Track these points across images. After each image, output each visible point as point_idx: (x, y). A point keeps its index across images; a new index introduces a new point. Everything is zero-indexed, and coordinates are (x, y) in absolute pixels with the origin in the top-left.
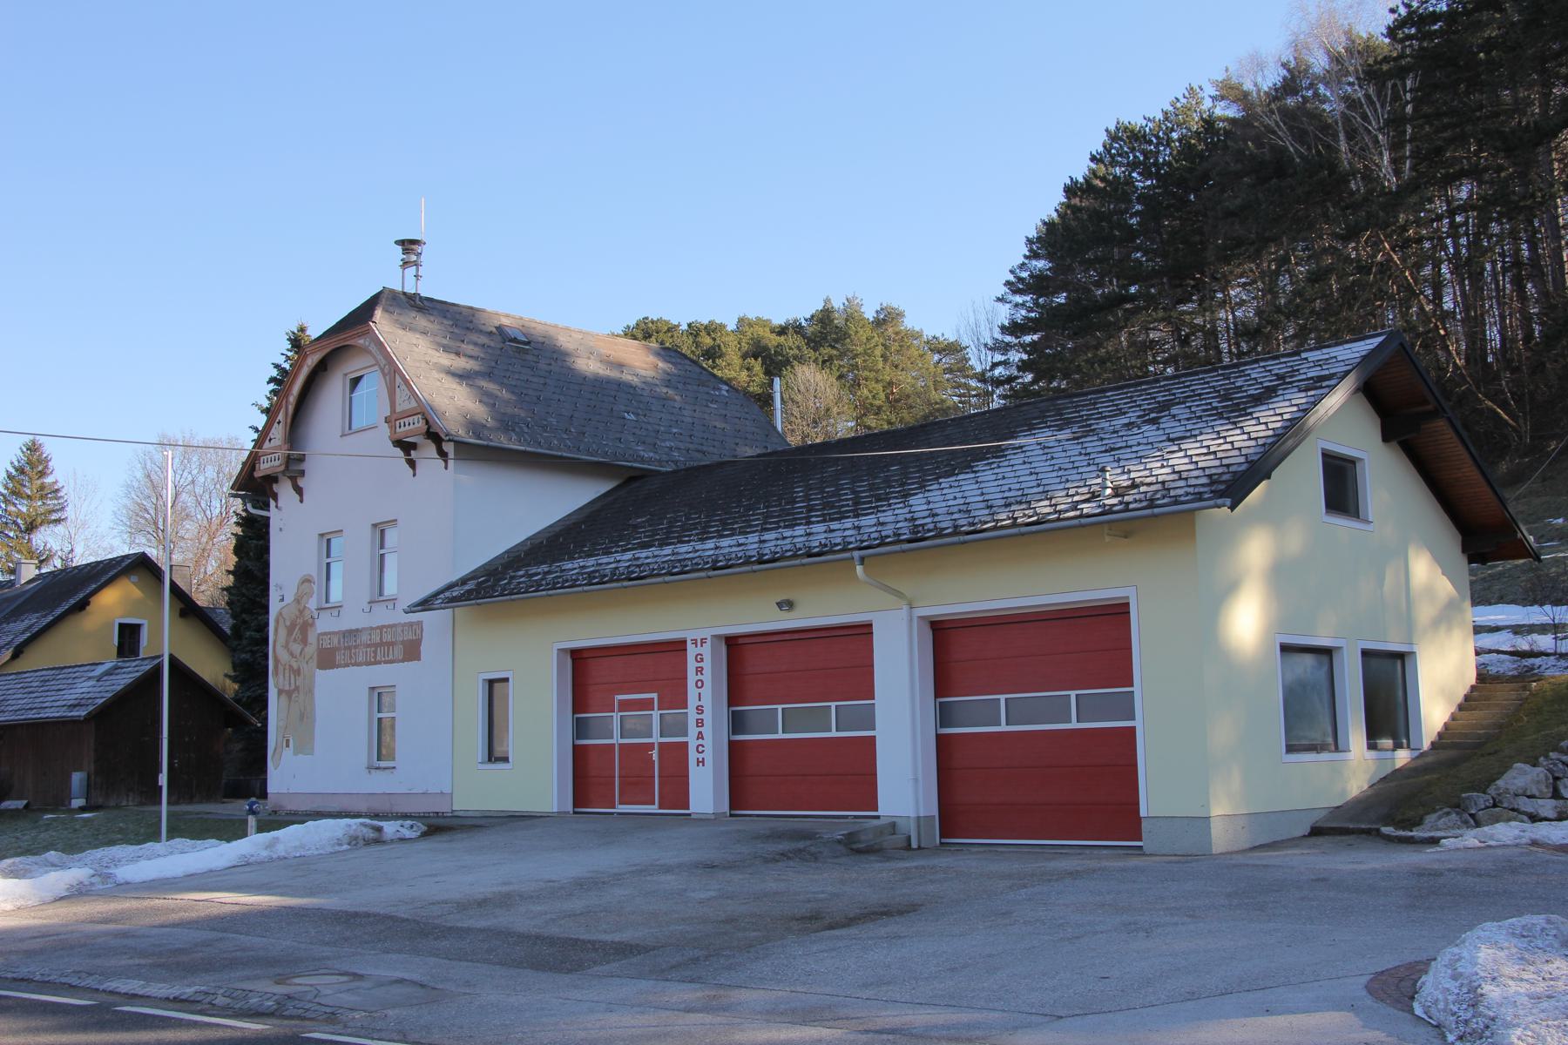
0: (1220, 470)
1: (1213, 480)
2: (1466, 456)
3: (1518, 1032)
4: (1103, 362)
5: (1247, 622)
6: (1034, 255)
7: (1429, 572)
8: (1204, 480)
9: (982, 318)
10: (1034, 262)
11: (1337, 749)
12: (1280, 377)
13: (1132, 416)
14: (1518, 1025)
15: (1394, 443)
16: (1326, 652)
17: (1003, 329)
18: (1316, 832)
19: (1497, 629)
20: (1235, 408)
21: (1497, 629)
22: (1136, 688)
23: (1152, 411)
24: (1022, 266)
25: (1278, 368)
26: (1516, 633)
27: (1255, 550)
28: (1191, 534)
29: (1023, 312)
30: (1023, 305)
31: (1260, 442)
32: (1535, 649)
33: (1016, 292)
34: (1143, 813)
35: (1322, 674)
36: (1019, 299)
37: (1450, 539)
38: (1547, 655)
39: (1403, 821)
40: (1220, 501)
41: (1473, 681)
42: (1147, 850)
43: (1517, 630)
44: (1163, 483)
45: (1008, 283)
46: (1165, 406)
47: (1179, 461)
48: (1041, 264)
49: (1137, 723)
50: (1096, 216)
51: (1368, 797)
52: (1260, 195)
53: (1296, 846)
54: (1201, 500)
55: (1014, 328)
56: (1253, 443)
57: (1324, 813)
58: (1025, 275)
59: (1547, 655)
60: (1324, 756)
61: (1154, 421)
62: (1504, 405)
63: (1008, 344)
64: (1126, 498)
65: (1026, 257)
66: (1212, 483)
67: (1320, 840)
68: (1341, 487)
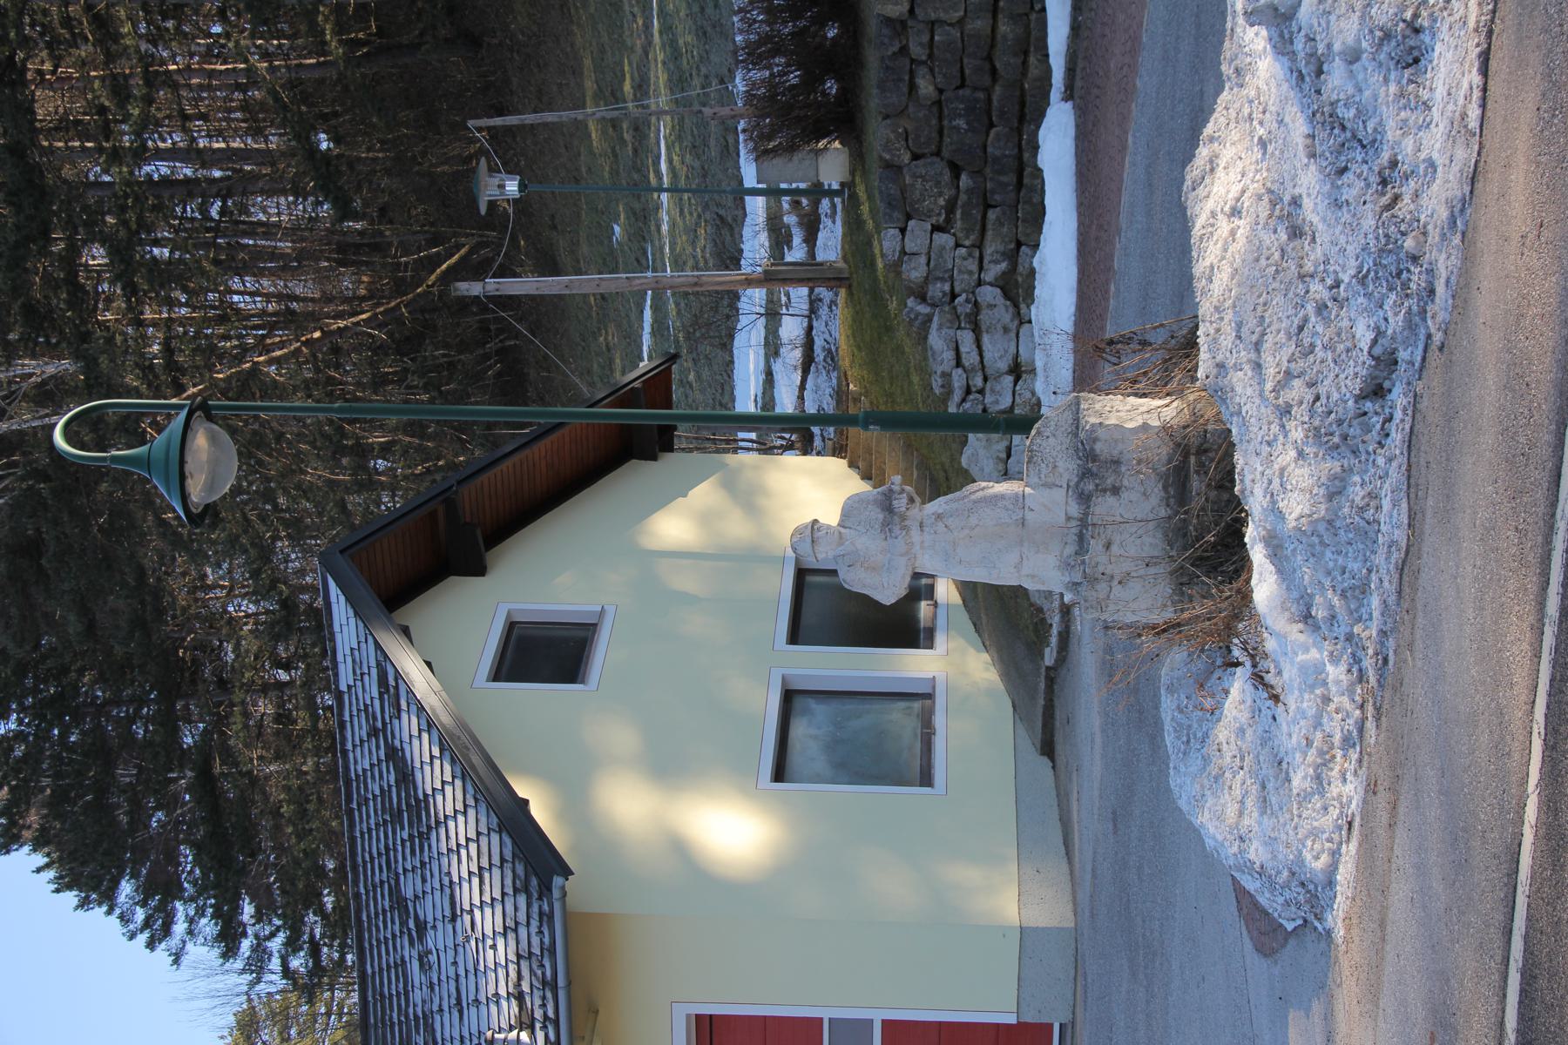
0: (509, 874)
1: (521, 888)
2: (516, 458)
3: (1308, 856)
4: (302, 814)
5: (734, 829)
6: (108, 897)
7: (681, 518)
8: (522, 900)
9: (203, 985)
10: (122, 898)
11: (930, 696)
12: (374, 732)
13: (410, 953)
14: (1300, 853)
15: (490, 556)
16: (789, 697)
17: (229, 952)
18: (1048, 748)
19: (769, 376)
20: (412, 811)
21: (769, 376)
22: (826, 1014)
23: (404, 923)
24: (125, 919)
25: (358, 729)
26: (777, 354)
27: (629, 804)
28: (602, 917)
29: (204, 921)
30: (191, 921)
31: (471, 802)
32: (799, 342)
33: (167, 930)
34: (1011, 1019)
35: (820, 709)
36: (180, 927)
37: (636, 477)
38: (810, 328)
39: (1036, 631)
40: (556, 894)
41: (843, 463)
42: (1065, 1017)
43: (772, 347)
44: (519, 956)
45: (151, 945)
46: (399, 903)
47: (489, 921)
48: (126, 888)
49: (878, 1017)
50: (57, 804)
51: (999, 651)
52: (66, 586)
53: (1067, 795)
54: (551, 916)
55: (228, 939)
56: (471, 813)
57: (1022, 731)
58: (140, 915)
59: (810, 328)
60: (939, 720)
61: (422, 927)
62: (435, 262)
63: (254, 949)
64: (538, 1014)
65: (109, 912)
66: (527, 891)
67: (1059, 748)
68: (547, 653)
